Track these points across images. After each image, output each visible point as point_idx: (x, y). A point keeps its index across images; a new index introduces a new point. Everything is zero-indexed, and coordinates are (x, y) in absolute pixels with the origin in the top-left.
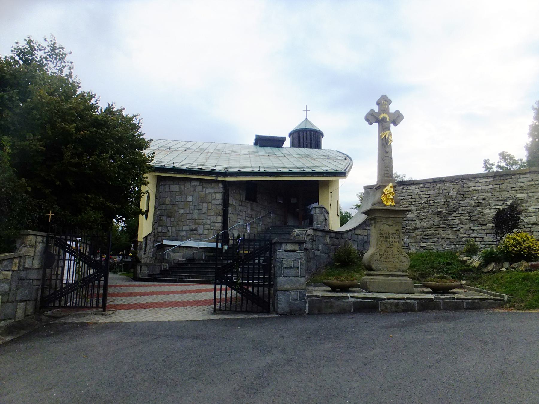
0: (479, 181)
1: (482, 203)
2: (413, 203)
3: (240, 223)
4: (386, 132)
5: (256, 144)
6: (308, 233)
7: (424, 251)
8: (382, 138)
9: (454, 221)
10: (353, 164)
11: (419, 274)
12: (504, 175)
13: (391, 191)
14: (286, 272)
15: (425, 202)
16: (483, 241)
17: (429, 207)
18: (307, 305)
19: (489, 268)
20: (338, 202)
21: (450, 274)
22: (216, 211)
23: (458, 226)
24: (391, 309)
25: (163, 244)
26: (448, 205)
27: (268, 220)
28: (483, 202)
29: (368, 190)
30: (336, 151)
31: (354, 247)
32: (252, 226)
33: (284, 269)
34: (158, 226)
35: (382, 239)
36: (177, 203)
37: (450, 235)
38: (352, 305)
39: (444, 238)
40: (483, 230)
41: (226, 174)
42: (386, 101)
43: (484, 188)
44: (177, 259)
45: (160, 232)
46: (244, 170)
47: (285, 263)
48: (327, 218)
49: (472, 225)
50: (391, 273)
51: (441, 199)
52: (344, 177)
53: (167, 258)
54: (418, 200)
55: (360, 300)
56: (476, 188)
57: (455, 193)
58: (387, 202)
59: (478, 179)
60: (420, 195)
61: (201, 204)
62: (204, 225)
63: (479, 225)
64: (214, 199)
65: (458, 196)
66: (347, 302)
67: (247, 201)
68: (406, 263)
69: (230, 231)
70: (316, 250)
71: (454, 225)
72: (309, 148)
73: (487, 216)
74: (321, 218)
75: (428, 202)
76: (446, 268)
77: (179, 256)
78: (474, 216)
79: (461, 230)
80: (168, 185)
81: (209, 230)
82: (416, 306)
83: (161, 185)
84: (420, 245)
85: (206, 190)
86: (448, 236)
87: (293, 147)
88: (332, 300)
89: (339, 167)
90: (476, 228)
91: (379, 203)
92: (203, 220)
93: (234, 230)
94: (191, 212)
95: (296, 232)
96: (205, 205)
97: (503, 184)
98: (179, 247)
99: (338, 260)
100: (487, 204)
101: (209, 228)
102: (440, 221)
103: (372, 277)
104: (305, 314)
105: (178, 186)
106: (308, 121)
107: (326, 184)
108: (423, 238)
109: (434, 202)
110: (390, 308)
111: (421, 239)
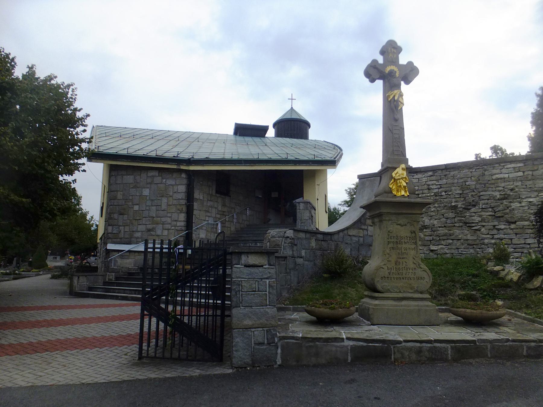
0: (505, 167)
1: (509, 195)
2: (420, 196)
3: (209, 222)
4: (396, 91)
5: (236, 133)
6: (286, 235)
7: (435, 256)
8: (389, 100)
9: (473, 218)
10: (342, 154)
11: (436, 290)
12: (539, 159)
13: (403, 174)
14: (247, 299)
15: (436, 195)
16: (512, 244)
17: (441, 201)
18: (279, 351)
19: (535, 283)
20: (326, 196)
21: (479, 290)
22: (178, 207)
23: (479, 224)
24: (409, 358)
25: (108, 248)
26: (465, 198)
27: (244, 217)
28: (511, 194)
29: (363, 180)
30: (324, 141)
31: (347, 251)
32: (224, 225)
33: (243, 295)
34: (108, 226)
35: (391, 245)
36: (131, 197)
37: (469, 236)
38: (349, 351)
39: (460, 240)
40: (512, 229)
41: (190, 162)
42: (394, 48)
43: (511, 176)
44: (126, 268)
45: (110, 233)
46: (212, 157)
47: (245, 285)
48: (313, 214)
49: (496, 223)
50: (405, 295)
51: (456, 190)
52: (334, 167)
53: (113, 266)
54: (426, 191)
55: (361, 343)
56: (502, 176)
57: (474, 183)
58: (398, 191)
59: (503, 164)
60: (429, 185)
61: (159, 198)
62: (163, 224)
63: (506, 223)
64: (175, 192)
65: (478, 186)
66: (344, 346)
67: (218, 195)
68: (427, 279)
69: (195, 231)
70: (298, 257)
71: (473, 223)
72: (295, 138)
73: (516, 212)
74: (306, 215)
75: (440, 194)
76: (472, 282)
77: (129, 263)
78: (499, 211)
79: (483, 230)
80: (120, 175)
81: (170, 231)
82: (449, 352)
83: (113, 175)
84: (430, 248)
85: (166, 181)
86: (465, 238)
87: (277, 137)
88: (317, 343)
89: (328, 156)
90: (503, 227)
91: (385, 192)
92: (162, 218)
93: (201, 230)
94: (148, 208)
95: (270, 234)
96: (165, 200)
97: (537, 170)
98: (129, 251)
99: (329, 271)
100: (515, 196)
101: (170, 227)
102: (454, 218)
103: (377, 302)
104: (275, 366)
105: (132, 177)
106: (294, 110)
107: (313, 174)
108: (433, 239)
109: (448, 194)
110: (408, 355)
111: (430, 241)
